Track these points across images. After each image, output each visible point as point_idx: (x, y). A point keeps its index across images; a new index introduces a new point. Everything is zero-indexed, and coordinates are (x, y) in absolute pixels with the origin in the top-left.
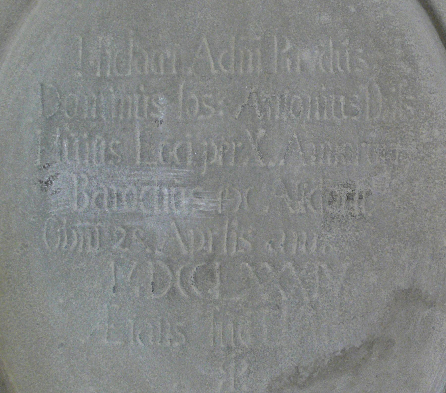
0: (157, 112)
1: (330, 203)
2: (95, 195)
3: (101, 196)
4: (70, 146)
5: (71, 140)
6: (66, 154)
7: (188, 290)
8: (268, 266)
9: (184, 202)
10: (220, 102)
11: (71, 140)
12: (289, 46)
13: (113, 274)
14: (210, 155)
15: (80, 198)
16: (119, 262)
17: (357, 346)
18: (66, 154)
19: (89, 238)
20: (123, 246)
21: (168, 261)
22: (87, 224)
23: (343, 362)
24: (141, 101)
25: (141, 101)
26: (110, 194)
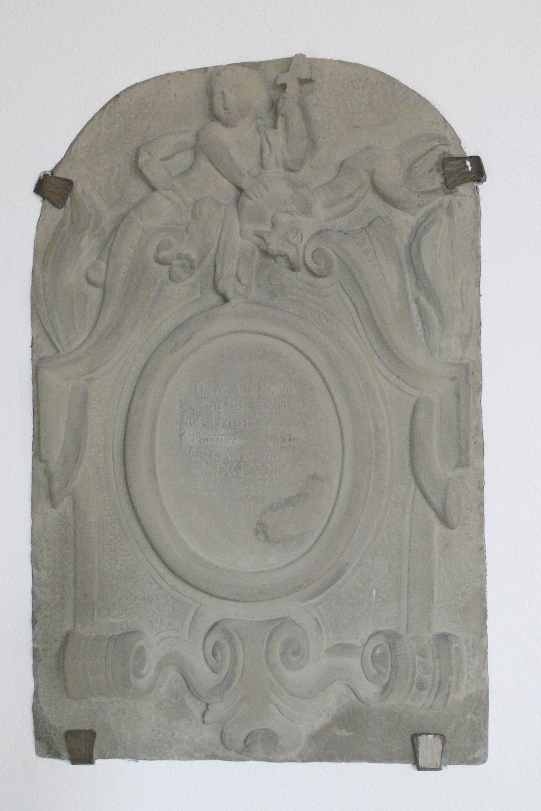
0: (220, 409)
1: (283, 442)
2: (199, 439)
3: (201, 439)
4: (190, 421)
5: (190, 419)
6: (189, 424)
7: (232, 473)
8: (260, 464)
9: (231, 441)
10: (243, 406)
11: (190, 419)
12: (267, 386)
13: (321, 623)
14: (239, 425)
15: (193, 440)
16: (207, 463)
17: (294, 495)
18: (189, 424)
19: (41, 292)
20: (209, 457)
21: (224, 463)
22: (196, 449)
23: (289, 502)
24: (215, 405)
25: (215, 405)
26: (204, 438)
